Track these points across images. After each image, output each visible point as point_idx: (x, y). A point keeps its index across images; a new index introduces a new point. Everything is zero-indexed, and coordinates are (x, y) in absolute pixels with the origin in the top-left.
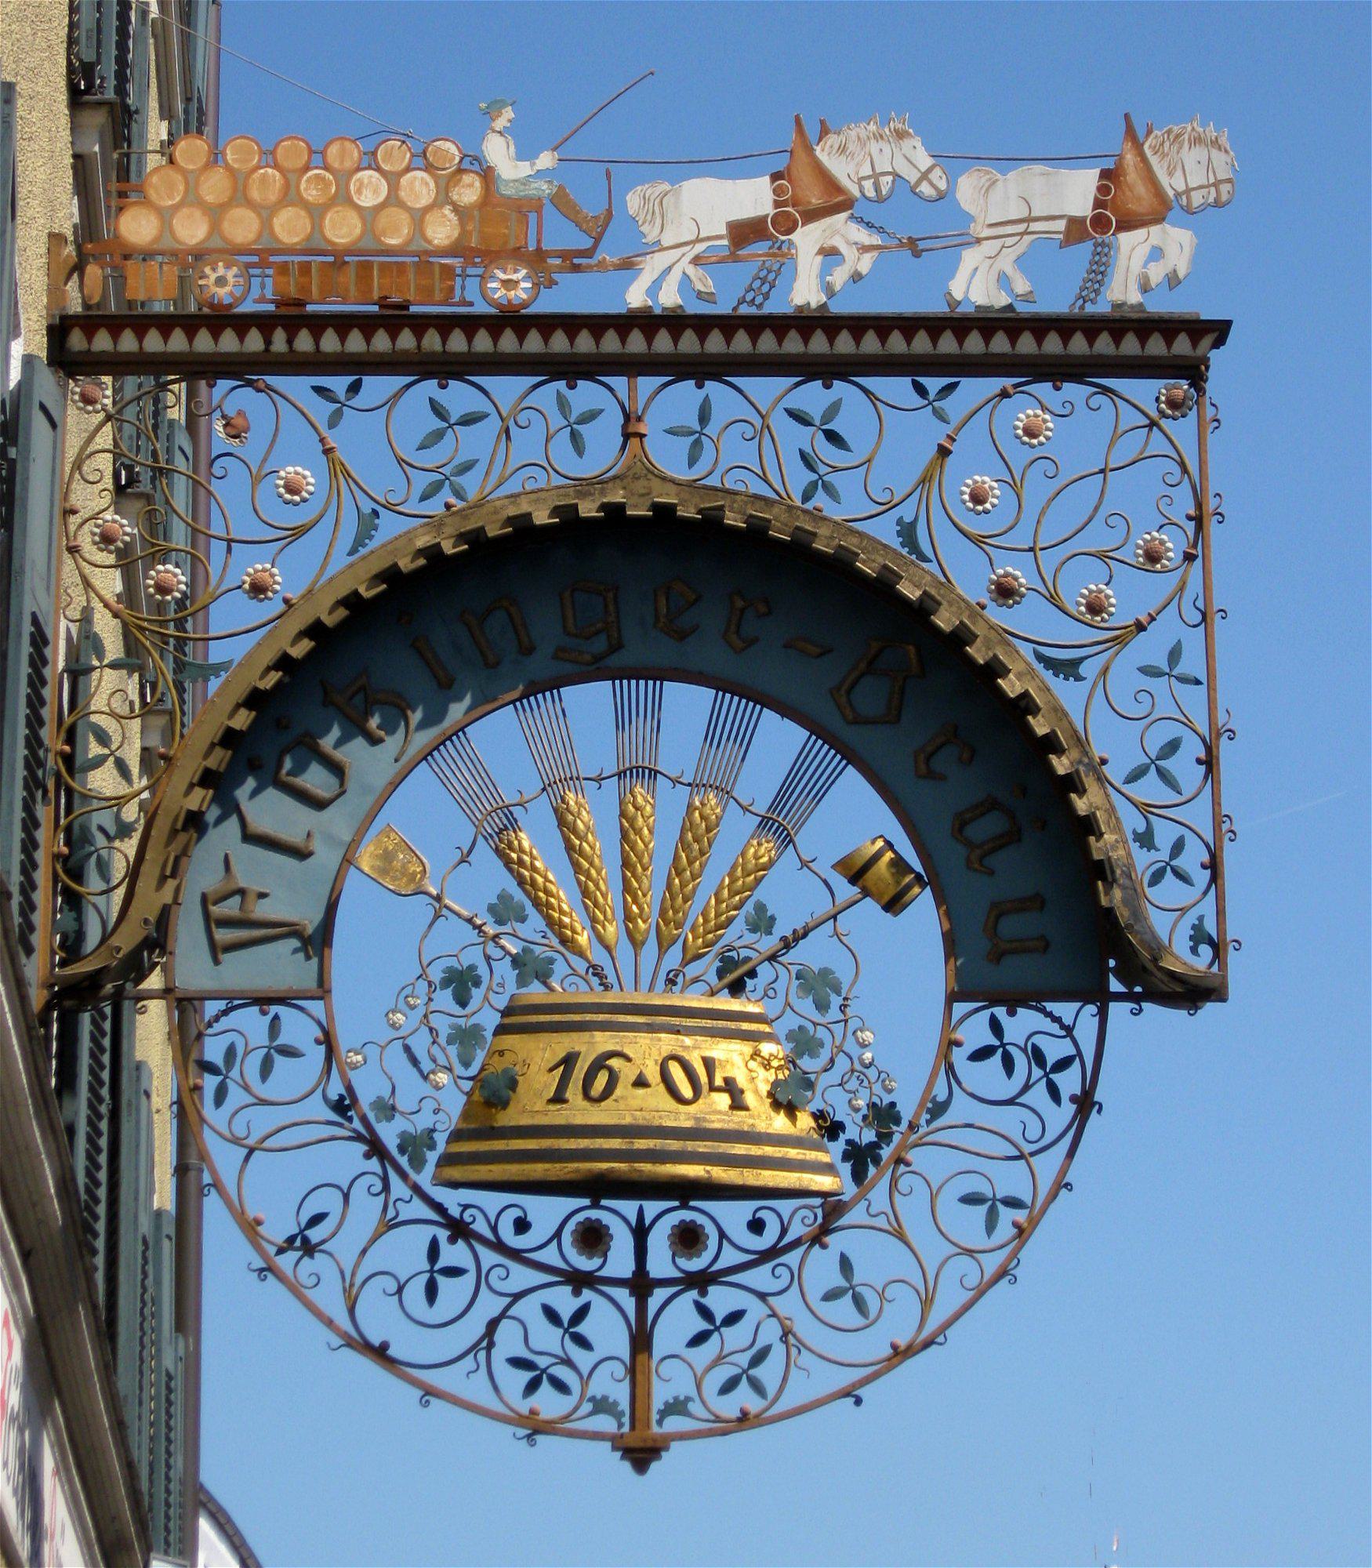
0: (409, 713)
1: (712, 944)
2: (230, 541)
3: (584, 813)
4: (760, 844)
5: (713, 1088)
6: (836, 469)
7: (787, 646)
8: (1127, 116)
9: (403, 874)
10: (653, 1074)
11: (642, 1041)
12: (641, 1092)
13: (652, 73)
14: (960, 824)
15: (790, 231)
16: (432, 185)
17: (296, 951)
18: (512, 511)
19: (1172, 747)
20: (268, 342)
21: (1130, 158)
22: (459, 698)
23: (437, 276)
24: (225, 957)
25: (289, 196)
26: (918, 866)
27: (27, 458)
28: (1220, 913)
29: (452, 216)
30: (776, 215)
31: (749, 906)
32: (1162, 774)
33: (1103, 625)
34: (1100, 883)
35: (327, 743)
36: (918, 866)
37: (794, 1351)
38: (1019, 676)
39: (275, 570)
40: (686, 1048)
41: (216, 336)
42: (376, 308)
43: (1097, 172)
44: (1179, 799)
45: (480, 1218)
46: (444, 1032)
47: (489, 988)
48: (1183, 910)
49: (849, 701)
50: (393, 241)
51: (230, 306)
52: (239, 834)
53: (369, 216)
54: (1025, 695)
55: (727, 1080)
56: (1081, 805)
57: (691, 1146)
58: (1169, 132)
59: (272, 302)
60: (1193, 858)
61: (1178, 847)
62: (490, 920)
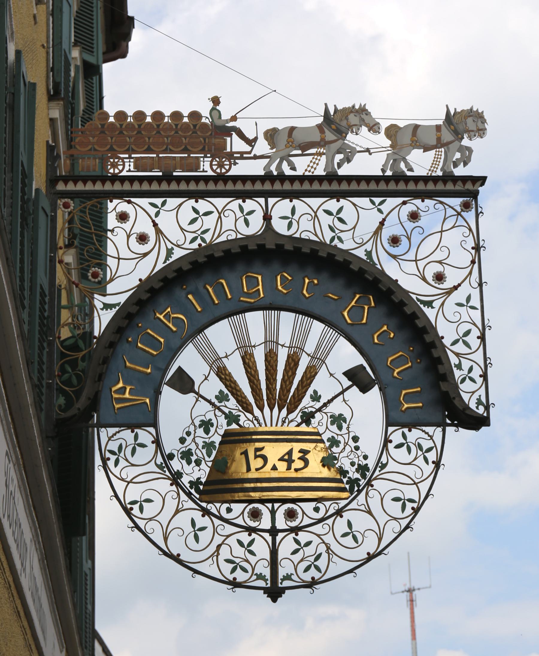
6: (342, 231)
47: (217, 426)
48: (473, 393)
60: (477, 373)
61: (471, 370)
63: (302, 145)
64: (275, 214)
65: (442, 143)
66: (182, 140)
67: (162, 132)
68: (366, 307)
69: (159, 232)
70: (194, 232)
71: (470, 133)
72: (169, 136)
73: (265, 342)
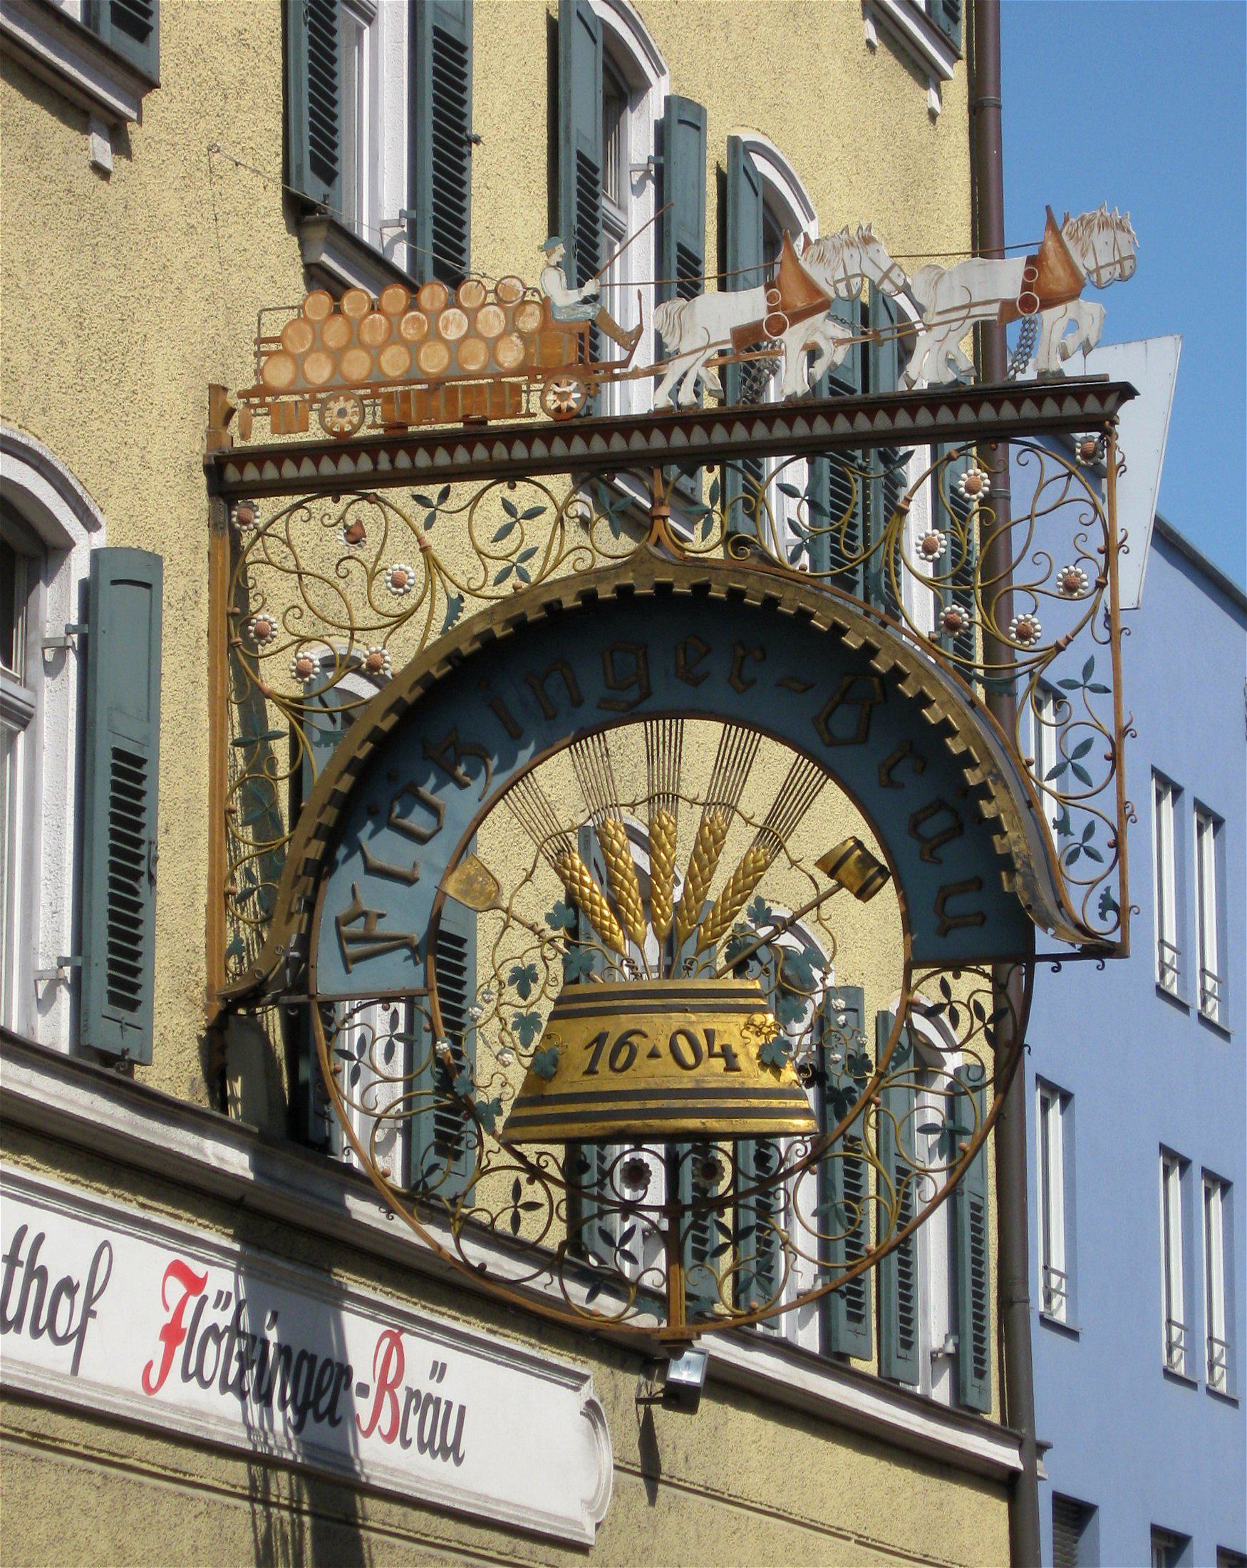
0: (488, 761)
1: (720, 935)
2: (352, 630)
3: (620, 834)
4: (758, 850)
5: (712, 1055)
7: (779, 685)
8: (1048, 208)
9: (481, 894)
10: (664, 1048)
11: (656, 1020)
12: (654, 1062)
14: (914, 826)
15: (780, 333)
16: (502, 316)
17: (407, 959)
18: (546, 598)
19: (1085, 747)
20: (375, 462)
21: (1051, 244)
22: (525, 746)
23: (507, 393)
24: (353, 967)
25: (393, 337)
26: (882, 860)
27: (96, 633)
28: (1123, 884)
29: (518, 342)
30: (769, 319)
31: (751, 901)
33: (1032, 647)
34: (1004, 874)
35: (425, 790)
36: (882, 860)
37: (792, 1256)
38: (942, 705)
39: (385, 652)
40: (691, 1023)
41: (336, 461)
42: (460, 425)
43: (1024, 259)
45: (551, 1162)
46: (511, 1021)
47: (546, 982)
48: (1093, 884)
49: (826, 725)
50: (473, 367)
51: (350, 433)
52: (363, 869)
53: (454, 347)
55: (723, 1047)
56: (988, 809)
57: (691, 1103)
58: (1082, 219)
59: (381, 426)
60: (1102, 839)
61: (1089, 831)
62: (547, 927)
69: (432, 564)
70: (505, 558)
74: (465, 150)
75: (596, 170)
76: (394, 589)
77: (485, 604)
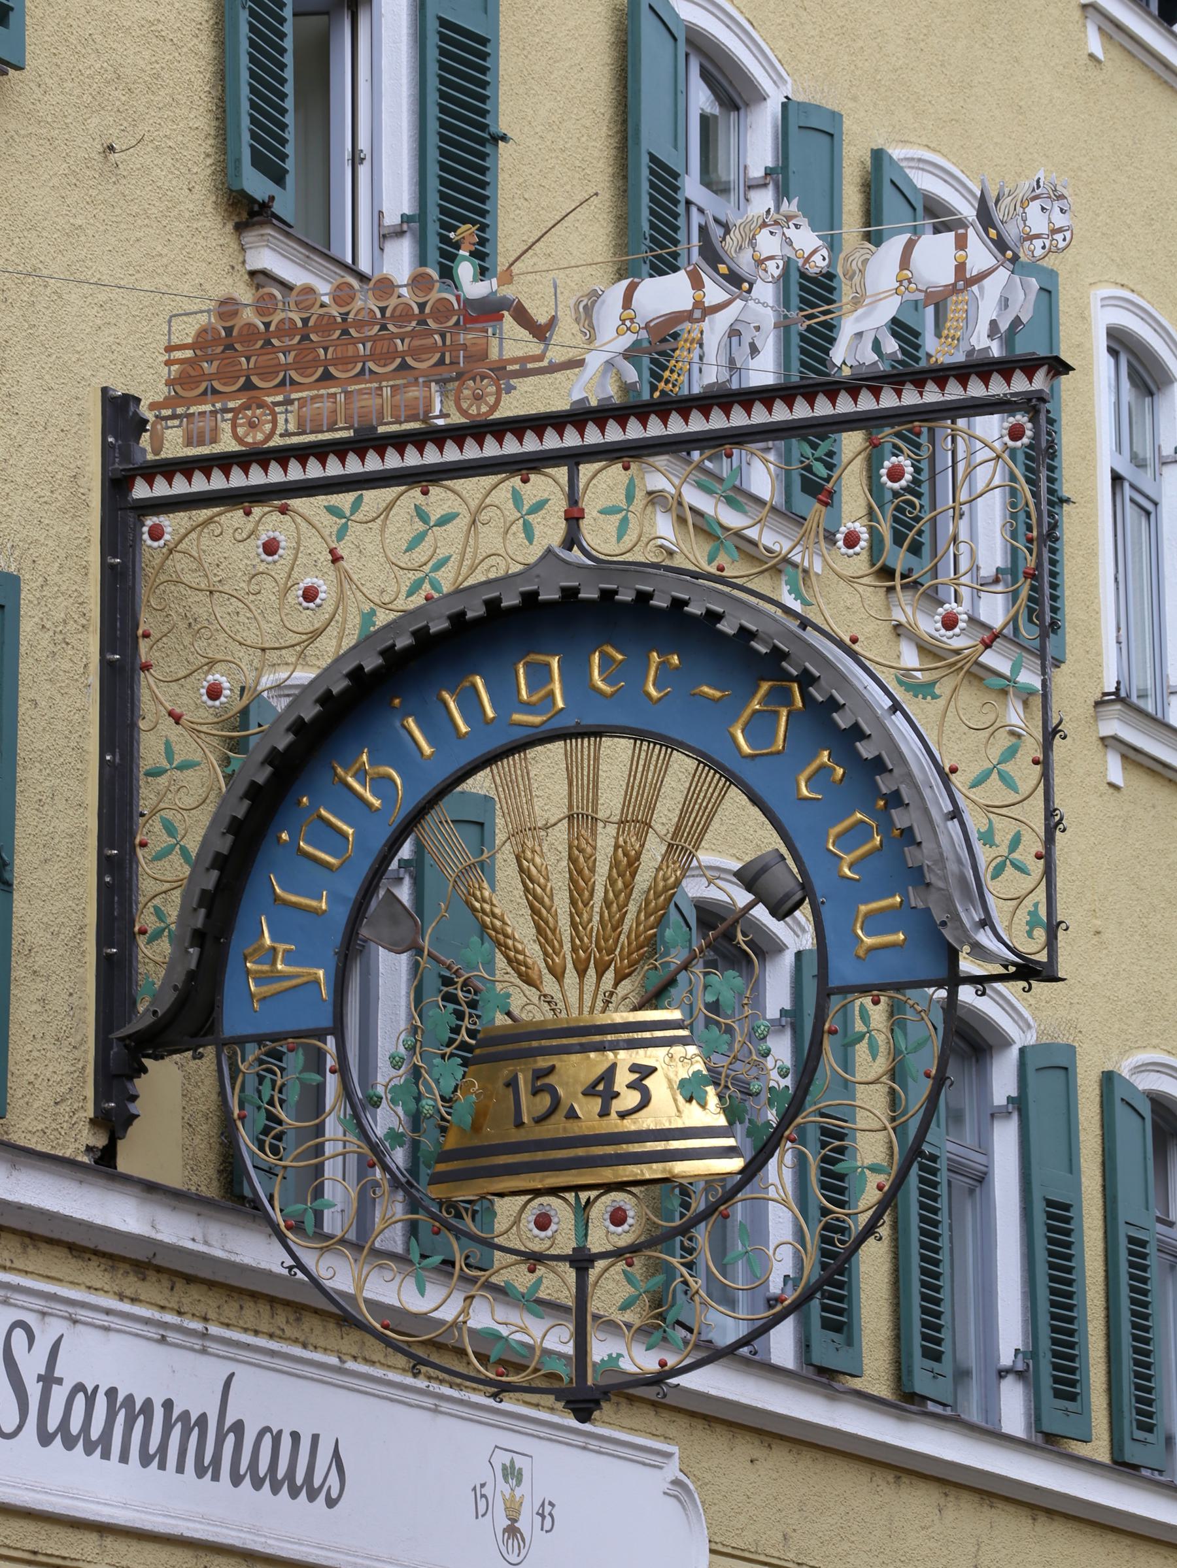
13: (596, 194)
32: (1003, 777)
38: (398, 635)
44: (1015, 798)
48: (1020, 899)
54: (414, 634)
63: (652, 324)
64: (591, 505)
65: (968, 276)
66: (396, 345)
67: (352, 331)
68: (784, 713)
71: (1034, 241)
72: (369, 338)
73: (570, 817)
74: (488, 149)
75: (676, 176)
76: (305, 604)
77: (392, 616)
